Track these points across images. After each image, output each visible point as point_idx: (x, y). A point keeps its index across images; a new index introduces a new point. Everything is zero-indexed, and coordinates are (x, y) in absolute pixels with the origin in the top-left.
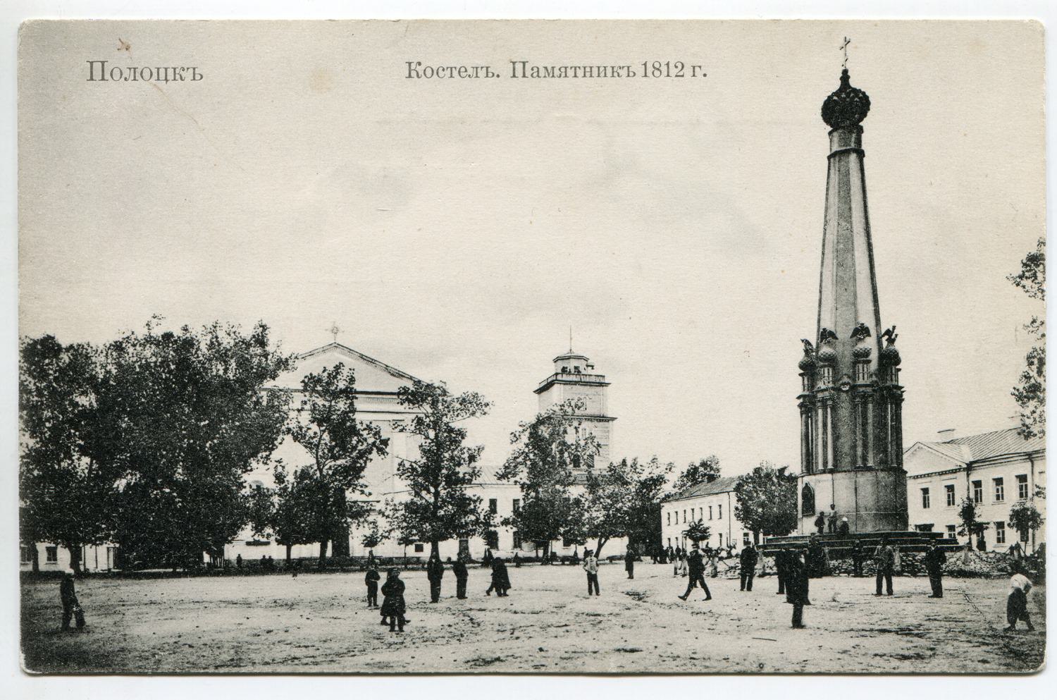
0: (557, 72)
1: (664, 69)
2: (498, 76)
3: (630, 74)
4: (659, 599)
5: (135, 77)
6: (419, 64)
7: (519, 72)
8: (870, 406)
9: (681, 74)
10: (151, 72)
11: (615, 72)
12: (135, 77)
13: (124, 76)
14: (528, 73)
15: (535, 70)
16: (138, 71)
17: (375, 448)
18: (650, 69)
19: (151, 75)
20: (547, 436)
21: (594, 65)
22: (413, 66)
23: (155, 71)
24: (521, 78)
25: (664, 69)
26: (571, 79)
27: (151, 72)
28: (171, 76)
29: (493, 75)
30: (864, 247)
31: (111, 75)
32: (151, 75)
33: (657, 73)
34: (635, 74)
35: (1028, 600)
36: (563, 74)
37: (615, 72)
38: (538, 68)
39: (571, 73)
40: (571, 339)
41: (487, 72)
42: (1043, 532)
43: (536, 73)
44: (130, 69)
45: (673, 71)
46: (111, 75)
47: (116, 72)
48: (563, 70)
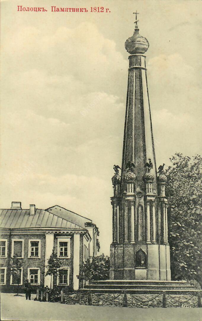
0: (65, 10)
1: (97, 9)
2: (47, 11)
3: (86, 11)
4: (86, 282)
7: (54, 10)
8: (136, 268)
9: (102, 11)
11: (81, 10)
14: (56, 10)
16: (34, 10)
17: (90, 263)
18: (93, 9)
19: (33, 10)
21: (20, 11)
25: (97, 9)
26: (69, 12)
29: (45, 10)
30: (152, 151)
32: (33, 10)
33: (95, 11)
34: (87, 11)
36: (67, 11)
37: (81, 10)
39: (69, 10)
43: (58, 10)
45: (100, 10)
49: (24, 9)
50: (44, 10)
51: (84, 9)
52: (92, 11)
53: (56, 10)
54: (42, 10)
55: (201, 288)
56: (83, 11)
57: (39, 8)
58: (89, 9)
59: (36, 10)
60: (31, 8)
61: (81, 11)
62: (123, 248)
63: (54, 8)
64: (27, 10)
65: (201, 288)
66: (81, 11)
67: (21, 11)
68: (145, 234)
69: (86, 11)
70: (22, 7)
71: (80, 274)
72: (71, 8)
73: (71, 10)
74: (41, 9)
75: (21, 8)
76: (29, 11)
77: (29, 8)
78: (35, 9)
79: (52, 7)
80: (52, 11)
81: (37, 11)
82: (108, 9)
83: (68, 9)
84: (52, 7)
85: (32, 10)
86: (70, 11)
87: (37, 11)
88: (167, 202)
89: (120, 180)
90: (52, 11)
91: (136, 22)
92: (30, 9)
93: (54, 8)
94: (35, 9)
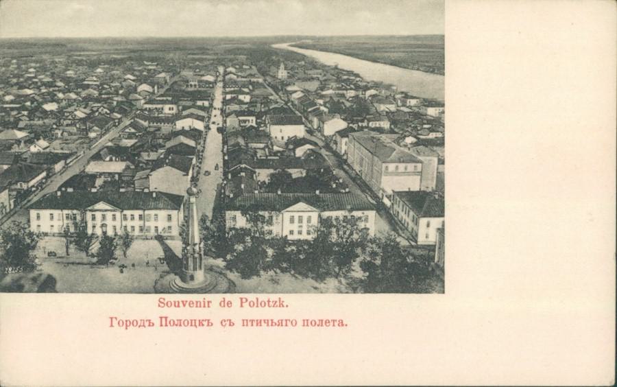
16: (256, 305)
24: (180, 301)
39: (250, 323)
48: (280, 322)
49: (172, 322)
50: (151, 324)
52: (112, 326)
54: (205, 323)
55: (62, 210)
56: (203, 325)
60: (265, 306)
63: (164, 320)
64: (176, 325)
65: (62, 210)
67: (166, 325)
68: (145, 44)
69: (210, 324)
70: (168, 320)
72: (334, 318)
73: (255, 324)
74: (204, 323)
75: (166, 320)
76: (322, 325)
77: (322, 320)
78: (193, 322)
80: (161, 325)
81: (196, 326)
82: (116, 318)
84: (161, 318)
86: (252, 325)
87: (196, 326)
89: (38, 65)
91: (133, 265)
93: (164, 320)
94: (193, 322)
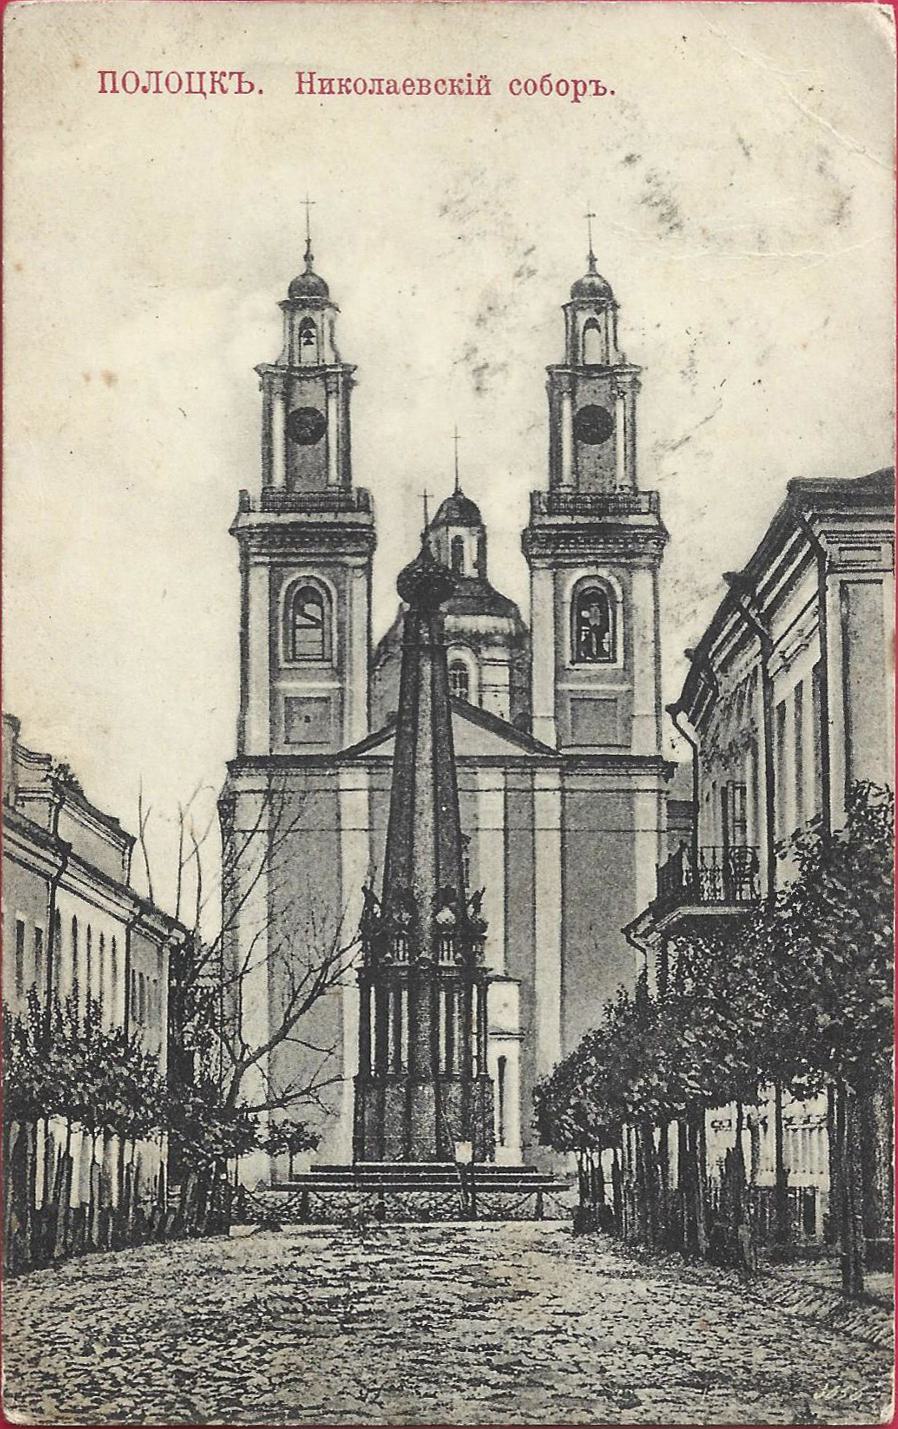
5: (114, 87)
6: (349, 80)
10: (180, 80)
12: (114, 87)
13: (141, 85)
15: (392, 83)
16: (185, 87)
20: (823, 1099)
22: (456, 83)
23: (185, 78)
27: (180, 80)
28: (336, 88)
31: (167, 84)
35: (352, 1082)
38: (395, 82)
40: (707, 419)
41: (240, 82)
42: (571, 573)
44: (150, 73)
46: (167, 84)
47: (131, 79)
51: (231, 74)
53: (384, 90)
57: (452, 81)
58: (499, 89)
59: (196, 87)
61: (453, 92)
62: (547, 779)
63: (108, 77)
66: (453, 92)
71: (401, 706)
74: (225, 81)
79: (103, 73)
83: (111, 88)
84: (103, 73)
85: (530, 92)
88: (772, 883)
90: (103, 90)
92: (185, 87)
